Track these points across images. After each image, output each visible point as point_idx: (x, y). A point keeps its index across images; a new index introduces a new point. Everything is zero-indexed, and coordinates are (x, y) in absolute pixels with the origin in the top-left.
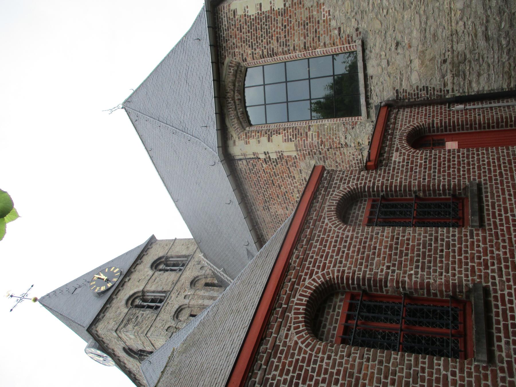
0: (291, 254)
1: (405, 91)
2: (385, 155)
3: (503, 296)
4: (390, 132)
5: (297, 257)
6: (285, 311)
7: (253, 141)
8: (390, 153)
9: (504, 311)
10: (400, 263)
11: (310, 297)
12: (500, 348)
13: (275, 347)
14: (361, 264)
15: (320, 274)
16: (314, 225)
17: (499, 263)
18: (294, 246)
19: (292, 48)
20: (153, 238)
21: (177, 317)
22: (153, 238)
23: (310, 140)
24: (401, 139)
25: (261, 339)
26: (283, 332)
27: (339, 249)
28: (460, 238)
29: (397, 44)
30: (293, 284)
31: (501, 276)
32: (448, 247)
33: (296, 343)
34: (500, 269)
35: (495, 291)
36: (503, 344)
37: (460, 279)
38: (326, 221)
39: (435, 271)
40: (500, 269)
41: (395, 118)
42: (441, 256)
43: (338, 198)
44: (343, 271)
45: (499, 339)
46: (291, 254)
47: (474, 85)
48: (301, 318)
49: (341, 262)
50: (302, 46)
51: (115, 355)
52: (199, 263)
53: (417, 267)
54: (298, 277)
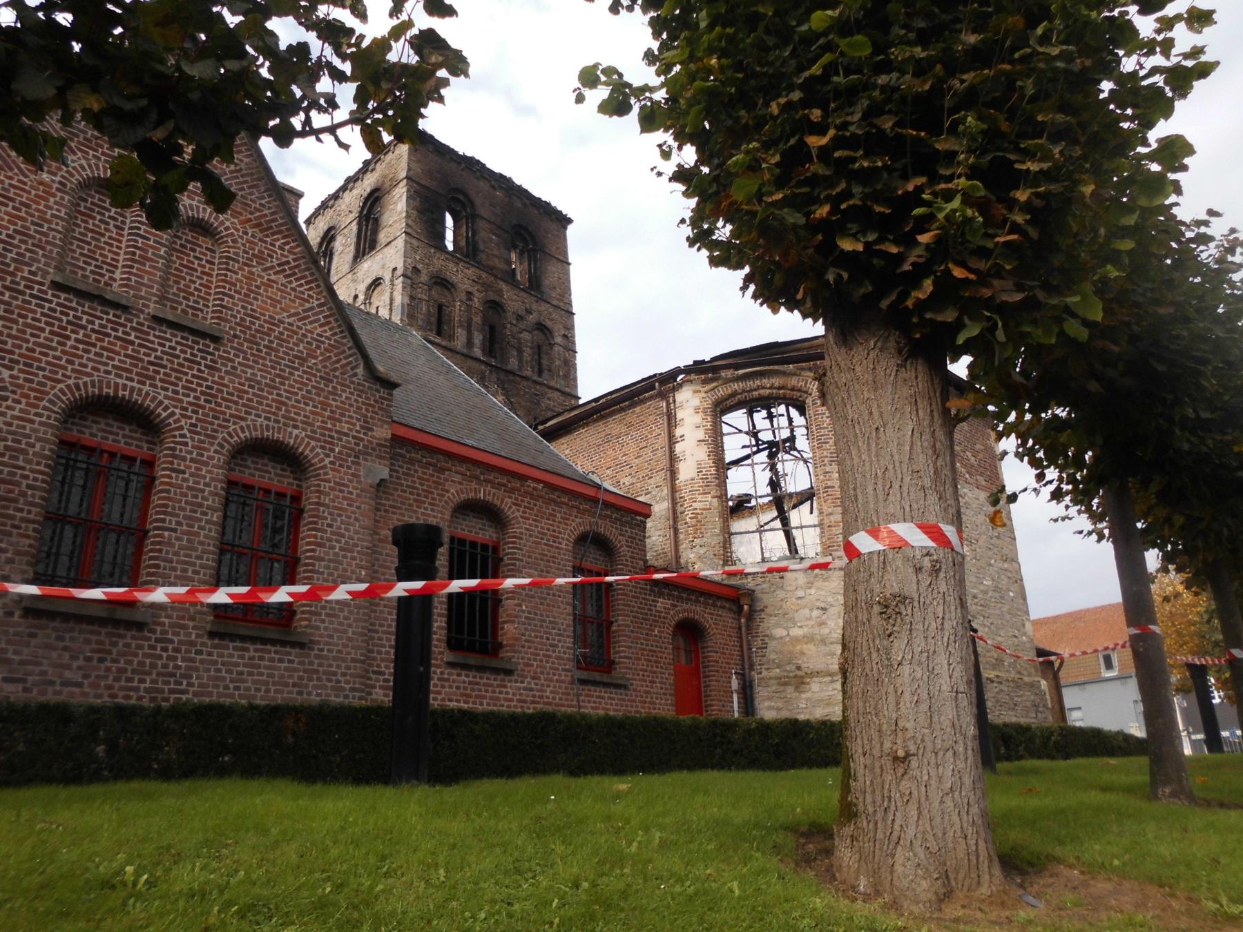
0: (539, 481)
1: (762, 620)
2: (666, 591)
3: (505, 687)
4: (702, 599)
5: (534, 489)
6: (477, 478)
7: (698, 419)
8: (670, 596)
9: (491, 685)
10: (532, 597)
11: (129, 401)
12: (459, 675)
13: (442, 470)
14: (530, 557)
15: (517, 514)
16: (573, 507)
17: (538, 691)
18: (548, 485)
19: (828, 469)
20: (570, 221)
21: (435, 283)
22: (570, 221)
23: (700, 498)
24: (689, 611)
25: (450, 455)
26: (458, 478)
27: (545, 534)
28: (562, 658)
29: (824, 609)
30: (504, 485)
31: (525, 689)
32: (551, 645)
33: (448, 491)
34: (531, 690)
35: (510, 681)
36: (463, 678)
37: (520, 652)
38: (578, 520)
39: (526, 629)
40: (531, 690)
41: (723, 607)
42: (542, 637)
43: (607, 533)
44: (521, 538)
45: (467, 676)
46: (539, 481)
47: (767, 704)
48: (472, 495)
49: (531, 536)
50: (829, 484)
51: (364, 173)
52: (529, 312)
53: (529, 613)
54: (513, 490)
